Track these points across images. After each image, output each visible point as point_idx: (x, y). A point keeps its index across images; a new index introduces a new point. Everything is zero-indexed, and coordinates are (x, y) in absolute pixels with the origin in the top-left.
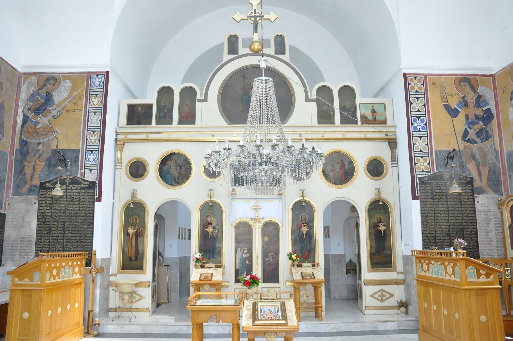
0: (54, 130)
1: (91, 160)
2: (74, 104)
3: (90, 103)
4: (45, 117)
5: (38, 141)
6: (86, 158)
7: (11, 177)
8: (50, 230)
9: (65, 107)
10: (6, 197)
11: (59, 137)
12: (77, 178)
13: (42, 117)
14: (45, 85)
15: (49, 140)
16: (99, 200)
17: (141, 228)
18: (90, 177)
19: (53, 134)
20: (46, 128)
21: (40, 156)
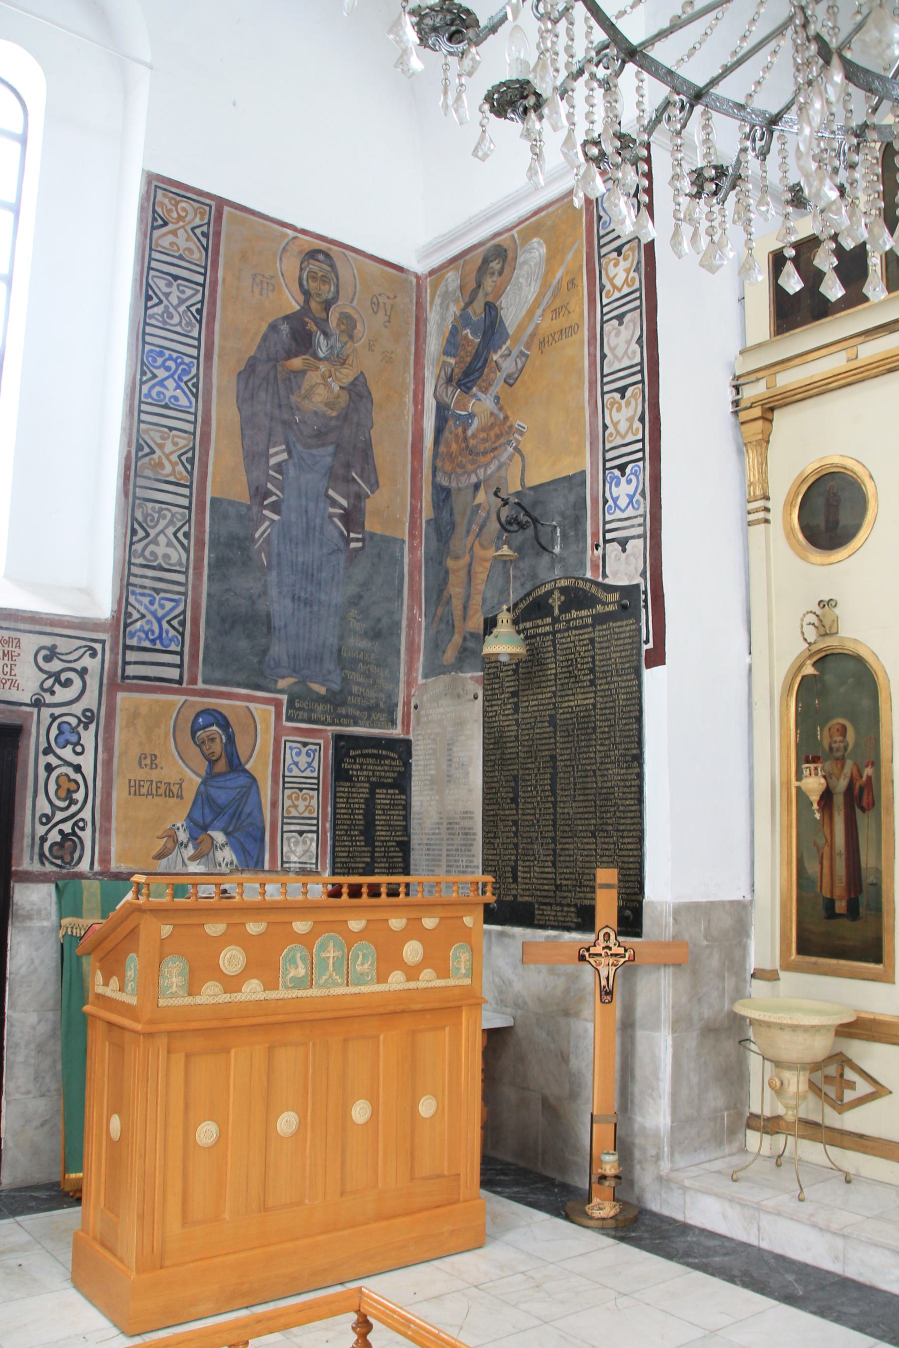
0: (511, 427)
1: (623, 502)
2: (557, 312)
3: (602, 287)
4: (485, 391)
5: (474, 479)
6: (605, 501)
7: (420, 616)
8: (515, 790)
9: (533, 335)
10: (409, 684)
11: (527, 447)
12: (581, 584)
13: (479, 394)
14: (479, 285)
15: (499, 468)
16: (657, 657)
17: (868, 771)
18: (623, 569)
19: (509, 442)
20: (492, 426)
21: (481, 528)
